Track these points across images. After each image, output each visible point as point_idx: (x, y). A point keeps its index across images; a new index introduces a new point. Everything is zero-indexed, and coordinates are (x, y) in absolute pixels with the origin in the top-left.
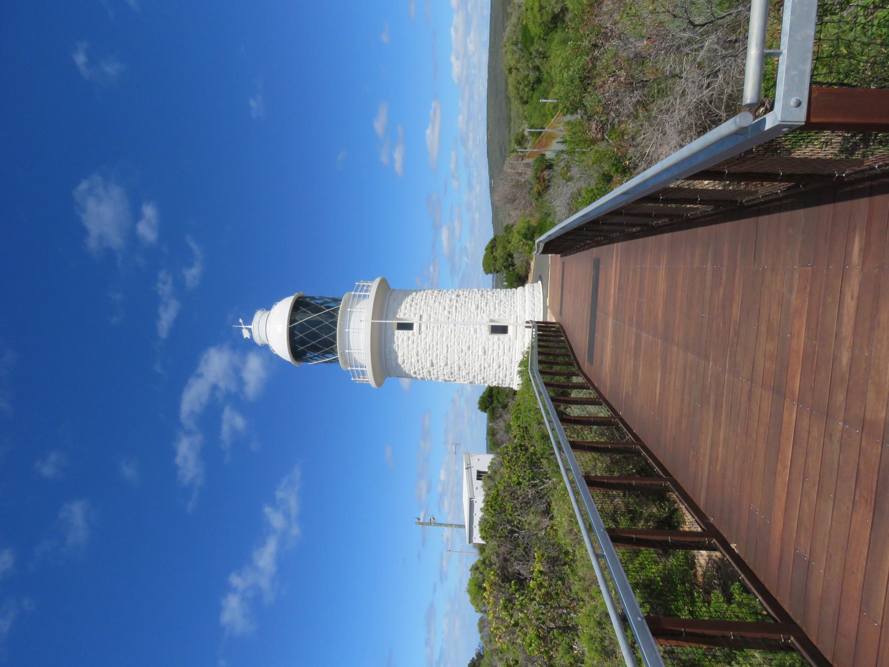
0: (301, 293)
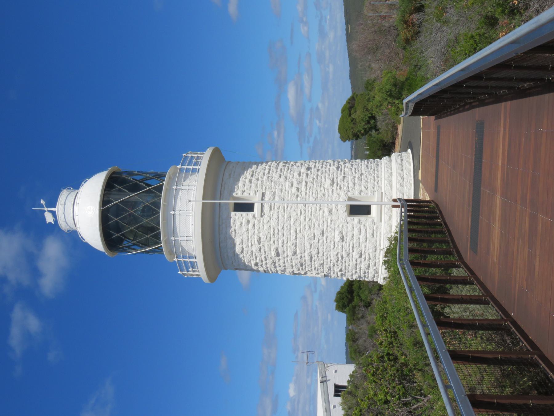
0: (116, 168)
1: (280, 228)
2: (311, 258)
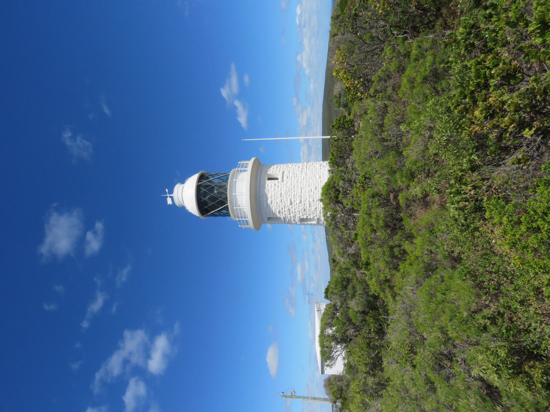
0: (204, 171)
1: (292, 187)
2: (310, 204)
